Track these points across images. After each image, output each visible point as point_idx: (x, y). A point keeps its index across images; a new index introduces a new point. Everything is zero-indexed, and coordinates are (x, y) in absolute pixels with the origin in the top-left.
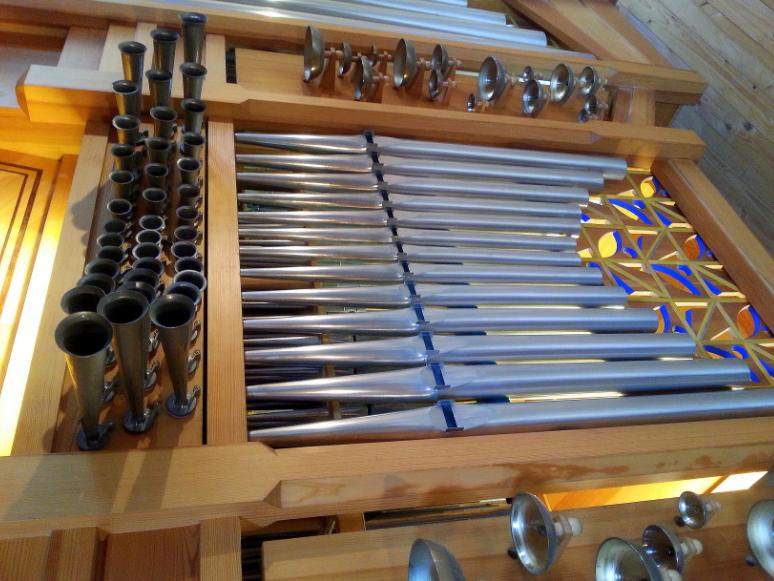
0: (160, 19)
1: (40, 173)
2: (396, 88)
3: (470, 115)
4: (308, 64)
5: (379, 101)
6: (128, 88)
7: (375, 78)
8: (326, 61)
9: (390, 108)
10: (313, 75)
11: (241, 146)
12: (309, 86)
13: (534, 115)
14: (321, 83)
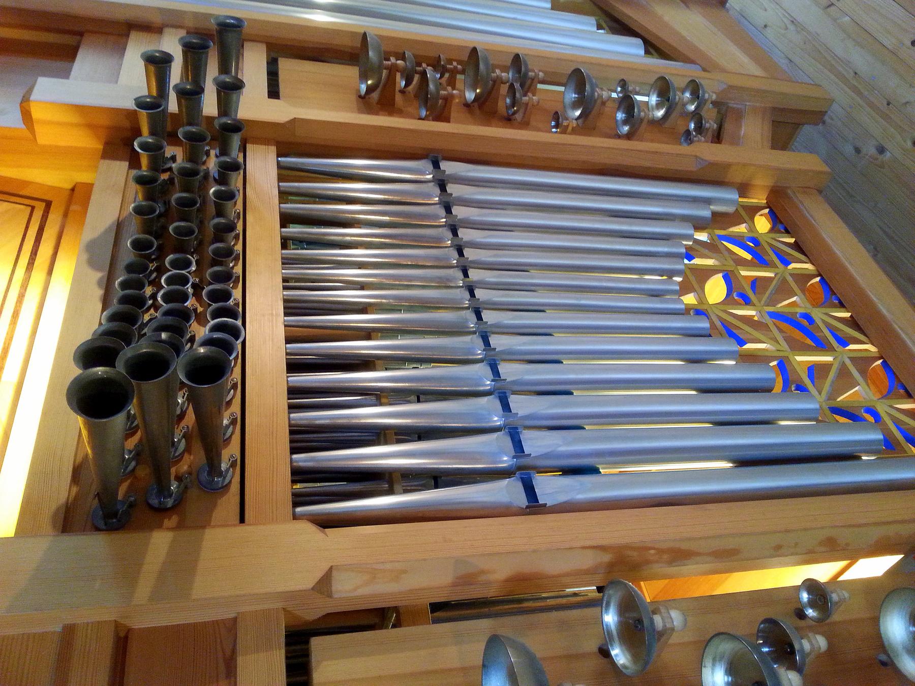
0: (190, 23)
1: (48, 204)
2: (467, 105)
3: (553, 137)
4: (364, 77)
5: (447, 120)
6: (152, 105)
7: (443, 92)
8: (385, 72)
9: (460, 128)
10: (370, 90)
11: (285, 173)
12: (365, 102)
13: (629, 136)
14: (381, 99)
